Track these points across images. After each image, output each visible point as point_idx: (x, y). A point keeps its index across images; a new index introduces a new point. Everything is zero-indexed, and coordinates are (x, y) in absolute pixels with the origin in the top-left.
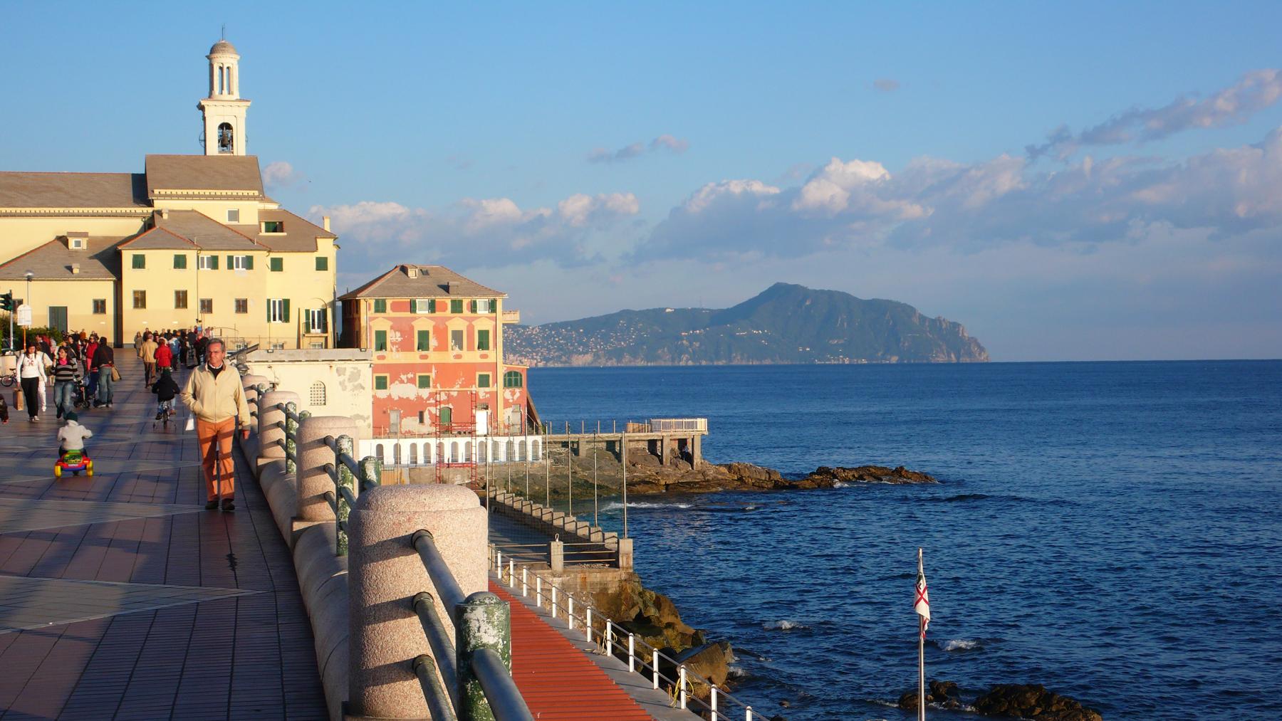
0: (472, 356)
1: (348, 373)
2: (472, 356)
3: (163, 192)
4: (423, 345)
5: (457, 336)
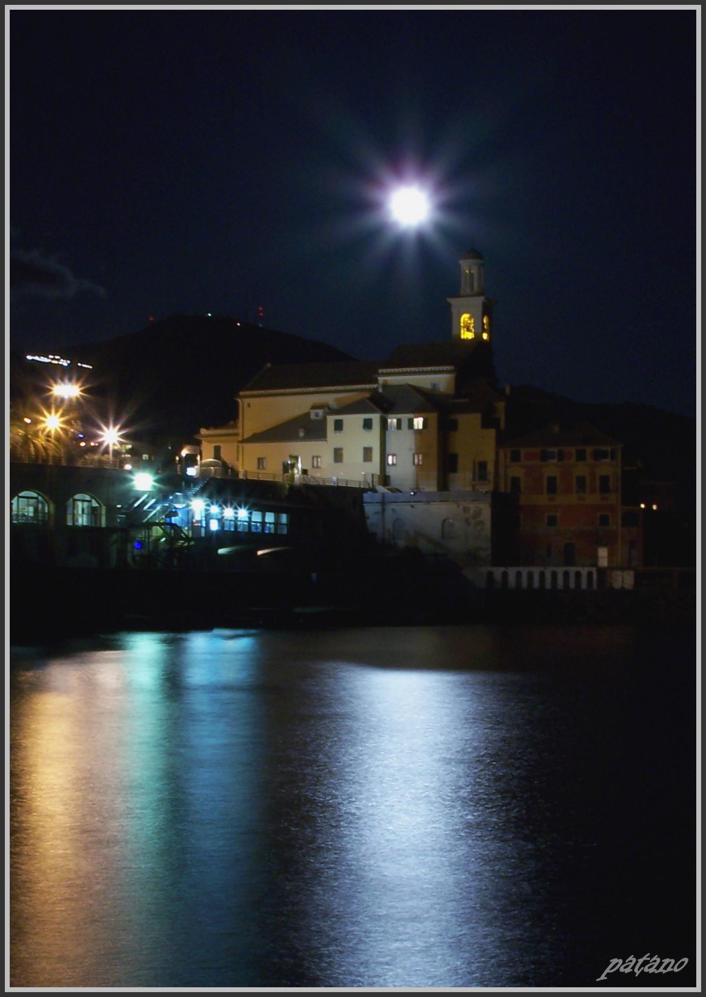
0: (593, 499)
1: (472, 512)
2: (593, 499)
3: (385, 371)
4: (552, 487)
5: (581, 481)
